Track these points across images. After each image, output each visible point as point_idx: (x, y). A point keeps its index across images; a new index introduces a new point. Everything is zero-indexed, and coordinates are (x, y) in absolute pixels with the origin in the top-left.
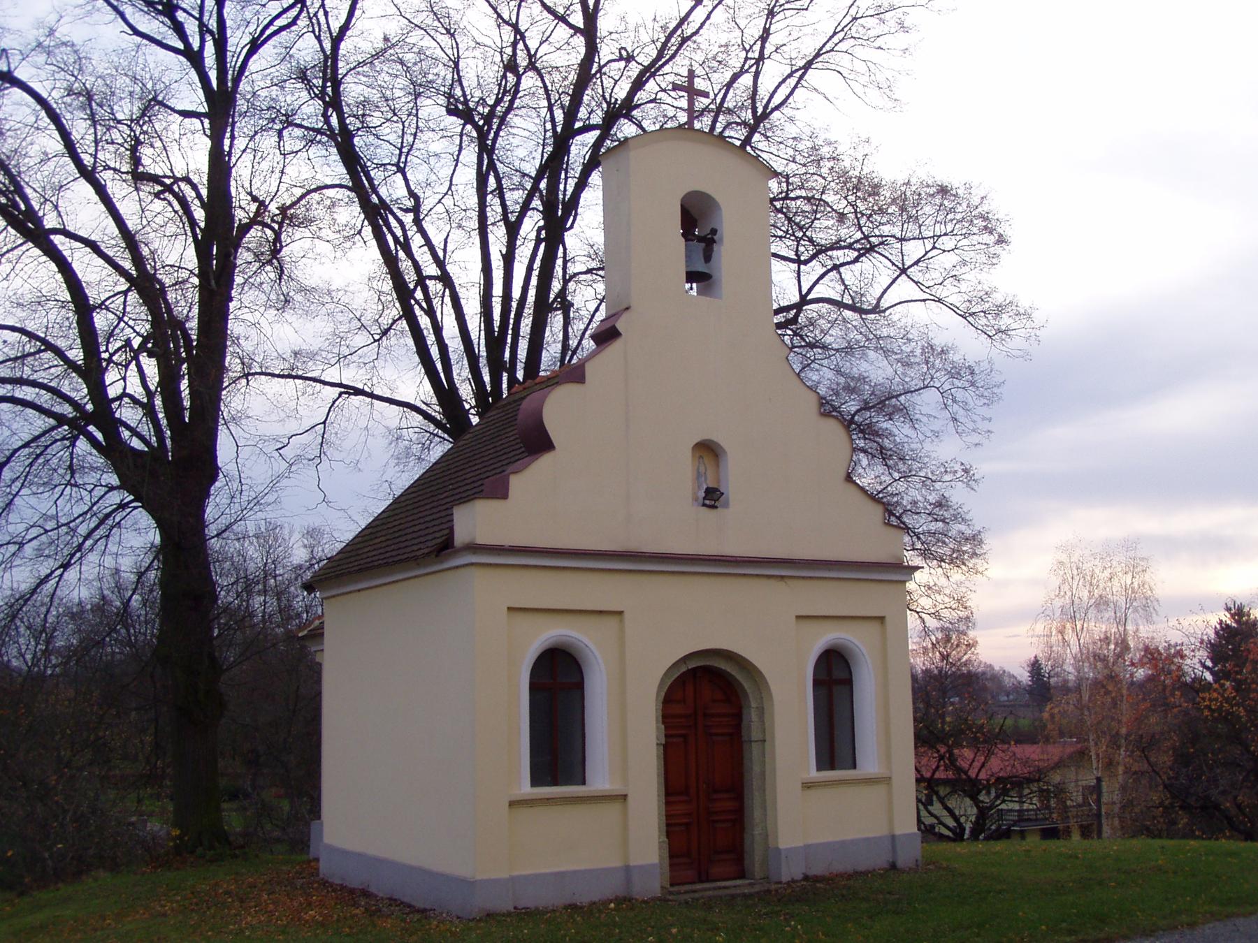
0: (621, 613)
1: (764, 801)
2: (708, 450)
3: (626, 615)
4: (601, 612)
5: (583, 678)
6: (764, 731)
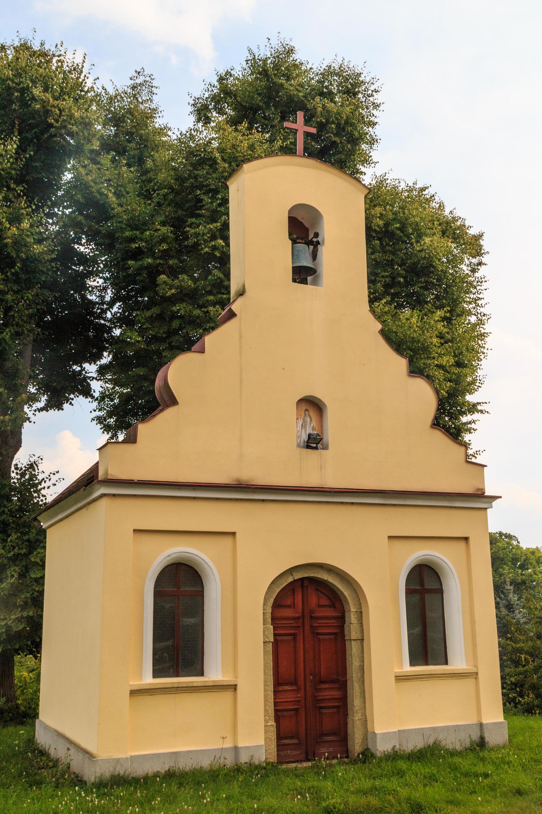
0: (234, 534)
1: (363, 692)
2: (312, 405)
3: (238, 535)
4: (474, 645)
5: (203, 588)
6: (362, 631)
